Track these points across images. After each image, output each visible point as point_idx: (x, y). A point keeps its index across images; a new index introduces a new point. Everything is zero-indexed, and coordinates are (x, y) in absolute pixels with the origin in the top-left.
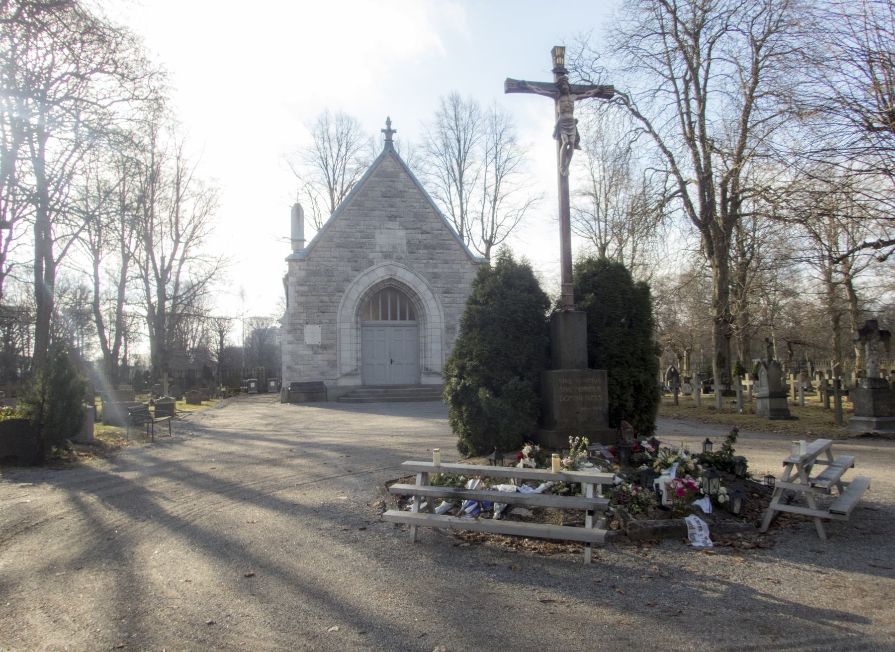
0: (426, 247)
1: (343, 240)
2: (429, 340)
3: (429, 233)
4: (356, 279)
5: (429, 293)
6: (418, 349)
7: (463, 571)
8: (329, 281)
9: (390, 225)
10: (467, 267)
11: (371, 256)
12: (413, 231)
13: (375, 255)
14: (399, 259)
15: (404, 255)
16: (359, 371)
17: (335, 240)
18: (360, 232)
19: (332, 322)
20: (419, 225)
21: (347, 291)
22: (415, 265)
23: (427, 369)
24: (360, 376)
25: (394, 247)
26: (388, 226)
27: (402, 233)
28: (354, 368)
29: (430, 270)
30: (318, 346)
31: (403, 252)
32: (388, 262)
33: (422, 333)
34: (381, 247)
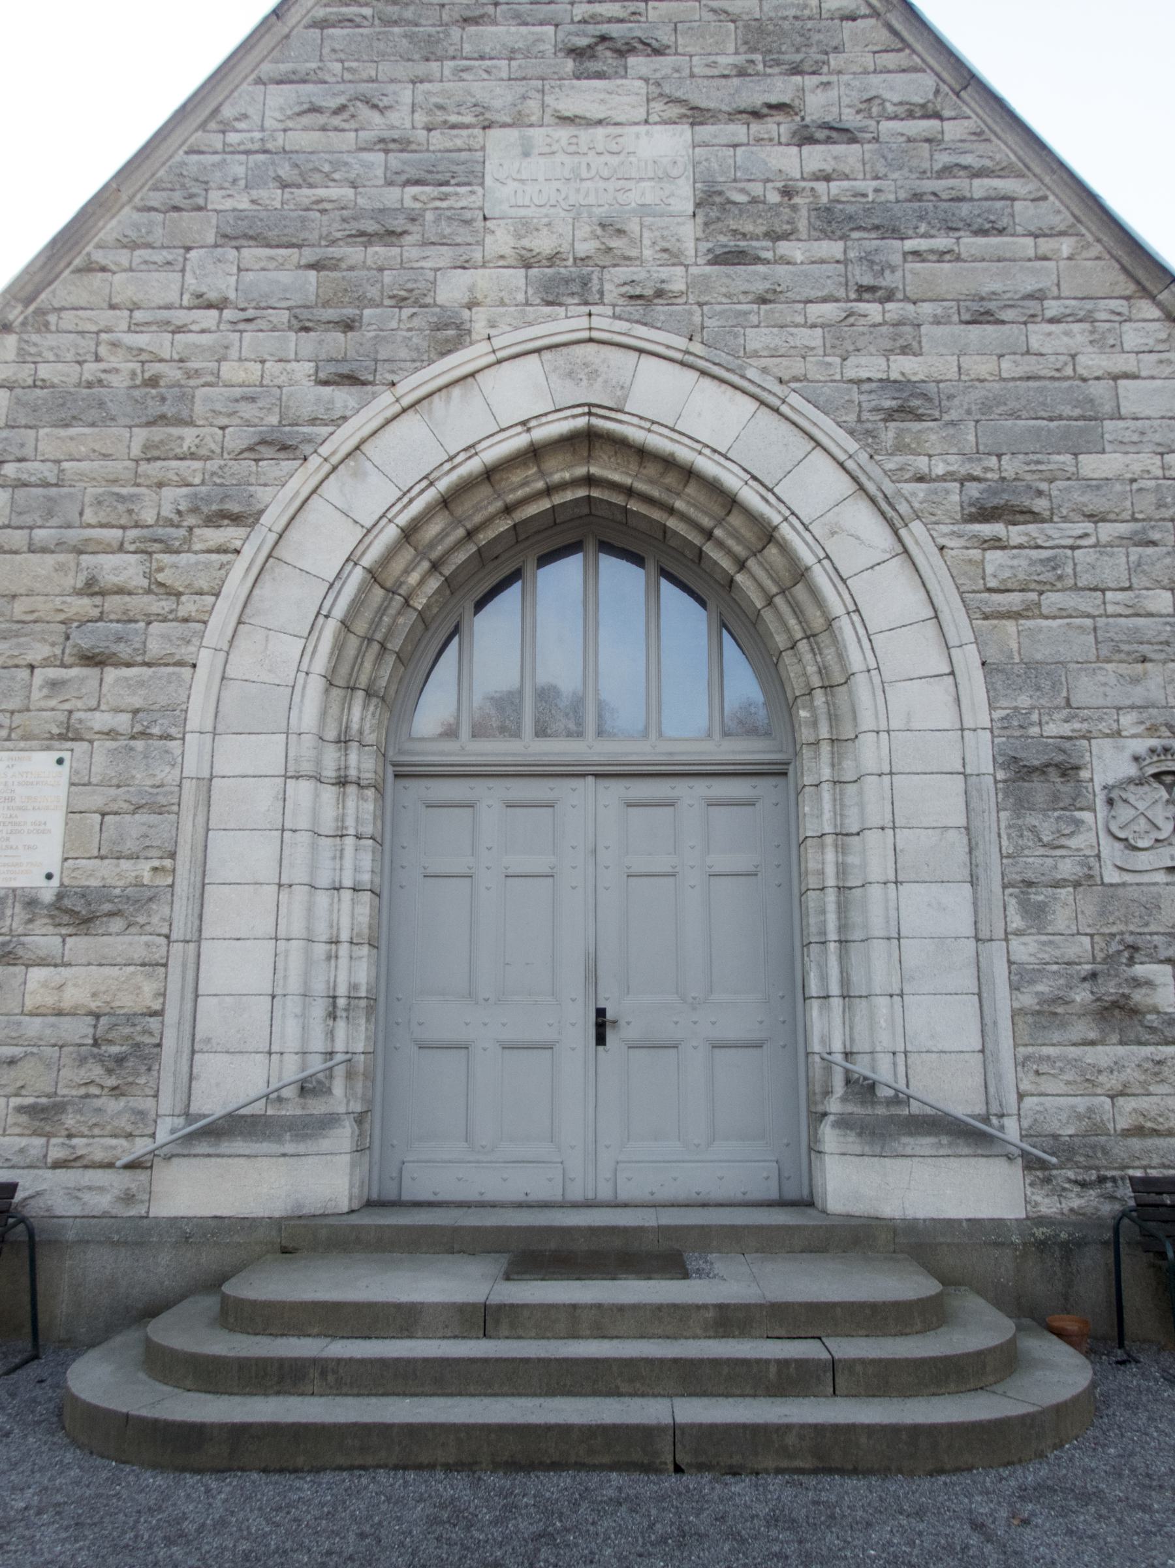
0: (831, 221)
1: (273, 196)
2: (874, 858)
3: (848, 135)
4: (343, 439)
5: (862, 520)
6: (798, 932)
7: (644, 210)
8: (152, 453)
9: (584, 97)
10: (1132, 337)
11: (451, 290)
12: (738, 131)
13: (482, 280)
14: (645, 300)
15: (677, 279)
16: (340, 1099)
17: (216, 199)
18: (384, 144)
19: (152, 729)
20: (781, 89)
21: (274, 518)
22: (758, 339)
23: (863, 1089)
24: (343, 1137)
25: (610, 227)
26: (569, 106)
27: (668, 143)
28: (291, 1071)
29: (869, 366)
30: (31, 903)
31: (672, 256)
32: (567, 322)
33: (819, 816)
34: (525, 227)
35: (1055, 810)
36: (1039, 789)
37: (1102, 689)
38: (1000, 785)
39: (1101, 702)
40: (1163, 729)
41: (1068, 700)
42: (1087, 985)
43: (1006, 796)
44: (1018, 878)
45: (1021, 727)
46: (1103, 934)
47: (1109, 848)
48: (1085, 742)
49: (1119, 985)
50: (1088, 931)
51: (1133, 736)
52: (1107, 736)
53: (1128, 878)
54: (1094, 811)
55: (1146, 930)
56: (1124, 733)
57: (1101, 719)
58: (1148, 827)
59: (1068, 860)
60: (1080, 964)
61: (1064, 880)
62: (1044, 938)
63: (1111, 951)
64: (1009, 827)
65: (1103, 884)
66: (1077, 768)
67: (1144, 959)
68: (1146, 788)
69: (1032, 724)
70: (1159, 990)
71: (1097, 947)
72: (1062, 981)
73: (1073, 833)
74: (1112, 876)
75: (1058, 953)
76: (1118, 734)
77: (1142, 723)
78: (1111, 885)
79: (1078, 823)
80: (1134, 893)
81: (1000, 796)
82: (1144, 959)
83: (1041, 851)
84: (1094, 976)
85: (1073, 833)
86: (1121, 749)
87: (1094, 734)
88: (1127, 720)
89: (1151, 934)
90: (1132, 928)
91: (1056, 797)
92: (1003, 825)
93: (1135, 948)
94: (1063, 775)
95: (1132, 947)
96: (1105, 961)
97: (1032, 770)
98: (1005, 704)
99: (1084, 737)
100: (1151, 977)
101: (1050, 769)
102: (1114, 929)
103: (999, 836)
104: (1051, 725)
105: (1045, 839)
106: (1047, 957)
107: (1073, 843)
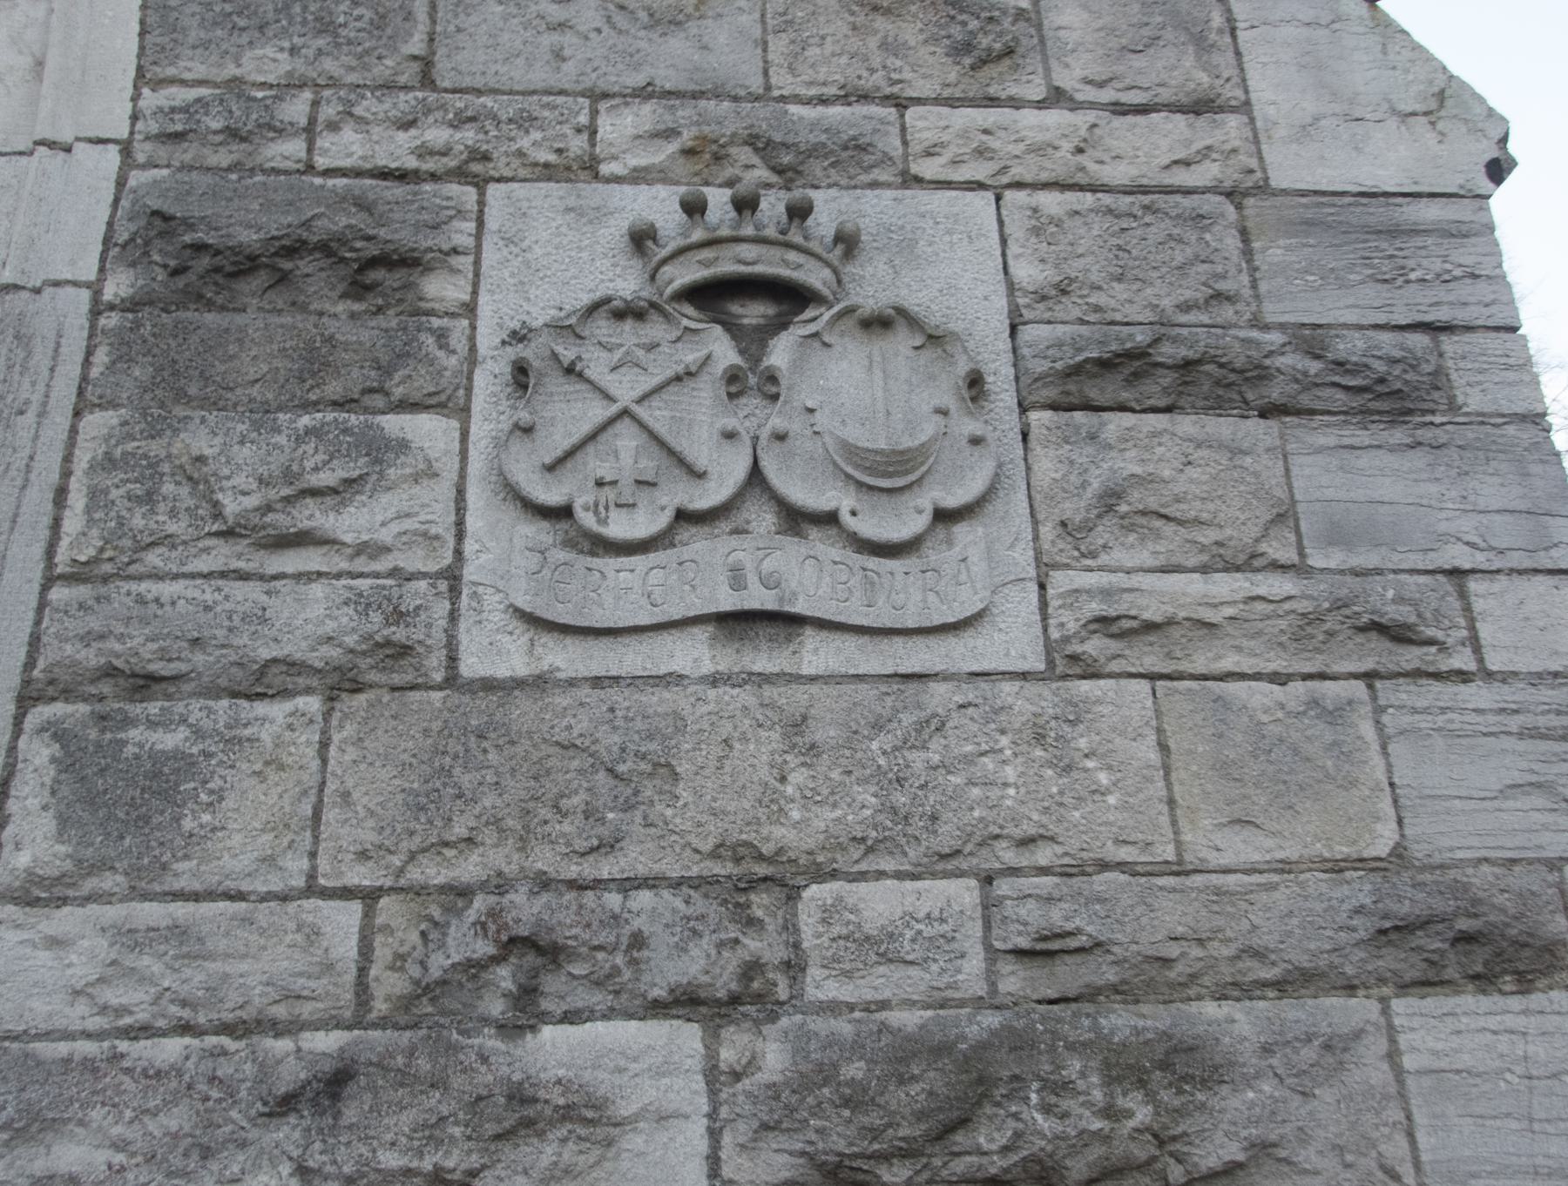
35: (308, 406)
36: (258, 333)
37: (548, 40)
38: (110, 321)
39: (540, 76)
40: (744, 154)
41: (426, 64)
42: (287, 1133)
43: (123, 357)
44: (91, 657)
45: (232, 134)
46: (419, 891)
47: (502, 552)
48: (467, 195)
49: (432, 1132)
50: (360, 876)
51: (638, 177)
52: (548, 173)
53: (564, 657)
54: (464, 412)
55: (606, 868)
56: (605, 169)
57: (525, 121)
58: (649, 465)
59: (317, 590)
60: (292, 1028)
61: (293, 666)
62: (152, 913)
63: (438, 963)
64: (108, 463)
65: (452, 680)
66: (409, 262)
67: (583, 997)
68: (656, 330)
69: (282, 132)
70: (634, 1141)
71: (383, 952)
72: (177, 1119)
73: (351, 484)
74: (492, 651)
75: (194, 979)
76: (590, 168)
77: (670, 133)
78: (489, 685)
79: (381, 451)
80: (578, 717)
81: (101, 357)
82: (583, 997)
83: (221, 555)
84: (335, 1082)
85: (351, 484)
86: (600, 214)
87: (501, 166)
88: (620, 127)
89: (628, 885)
90: (544, 859)
91: (315, 360)
92: (82, 459)
93: (543, 950)
94: (358, 289)
95: (528, 943)
96: (405, 1012)
97: (244, 265)
98: (199, 70)
99: (460, 174)
100: (602, 1082)
101: (305, 265)
102: (469, 869)
103: (61, 494)
104: (348, 134)
105: (232, 506)
106: (135, 999)
107: (350, 523)
